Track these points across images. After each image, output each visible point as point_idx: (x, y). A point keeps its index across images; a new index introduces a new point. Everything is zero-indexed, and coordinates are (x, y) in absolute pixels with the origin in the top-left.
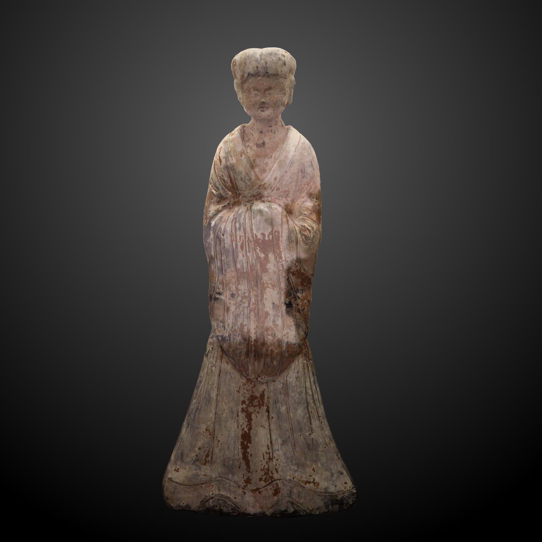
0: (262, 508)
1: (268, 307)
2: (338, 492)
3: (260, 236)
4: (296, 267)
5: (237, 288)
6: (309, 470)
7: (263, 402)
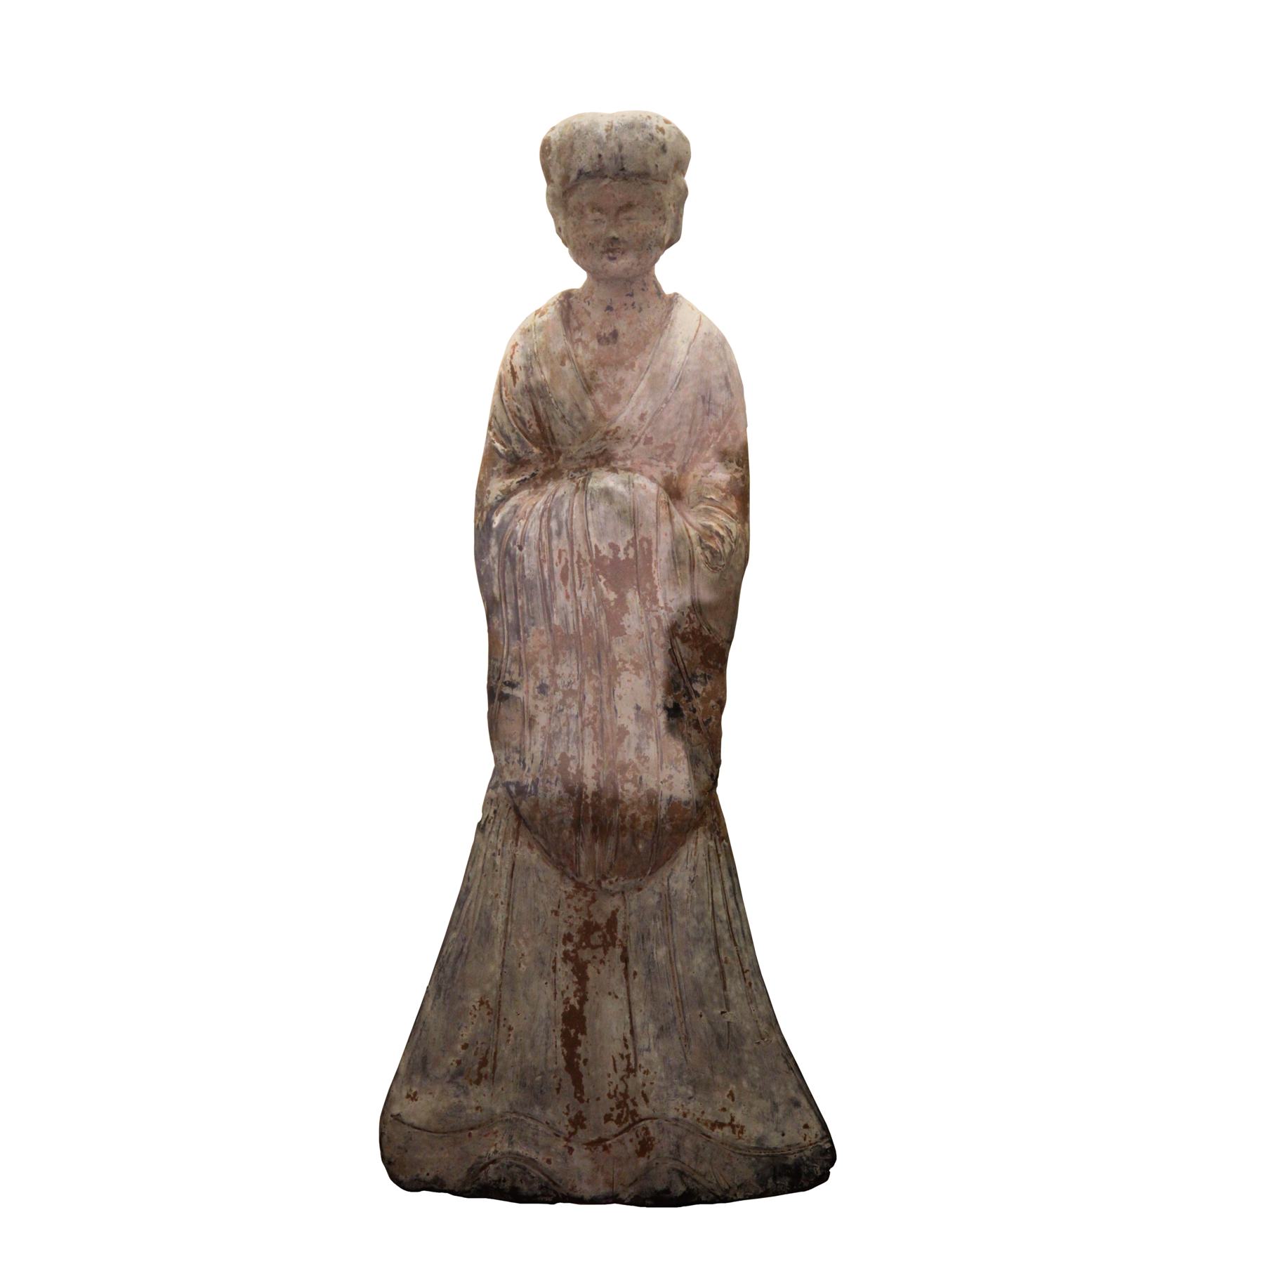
0: (612, 1185)
1: (626, 717)
2: (789, 1146)
3: (605, 551)
4: (691, 622)
5: (552, 672)
6: (720, 1097)
7: (614, 938)
